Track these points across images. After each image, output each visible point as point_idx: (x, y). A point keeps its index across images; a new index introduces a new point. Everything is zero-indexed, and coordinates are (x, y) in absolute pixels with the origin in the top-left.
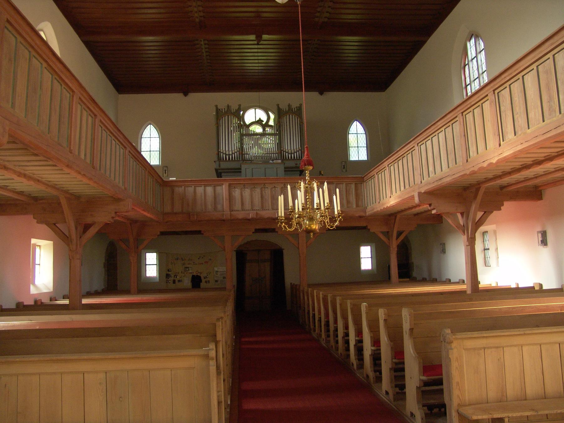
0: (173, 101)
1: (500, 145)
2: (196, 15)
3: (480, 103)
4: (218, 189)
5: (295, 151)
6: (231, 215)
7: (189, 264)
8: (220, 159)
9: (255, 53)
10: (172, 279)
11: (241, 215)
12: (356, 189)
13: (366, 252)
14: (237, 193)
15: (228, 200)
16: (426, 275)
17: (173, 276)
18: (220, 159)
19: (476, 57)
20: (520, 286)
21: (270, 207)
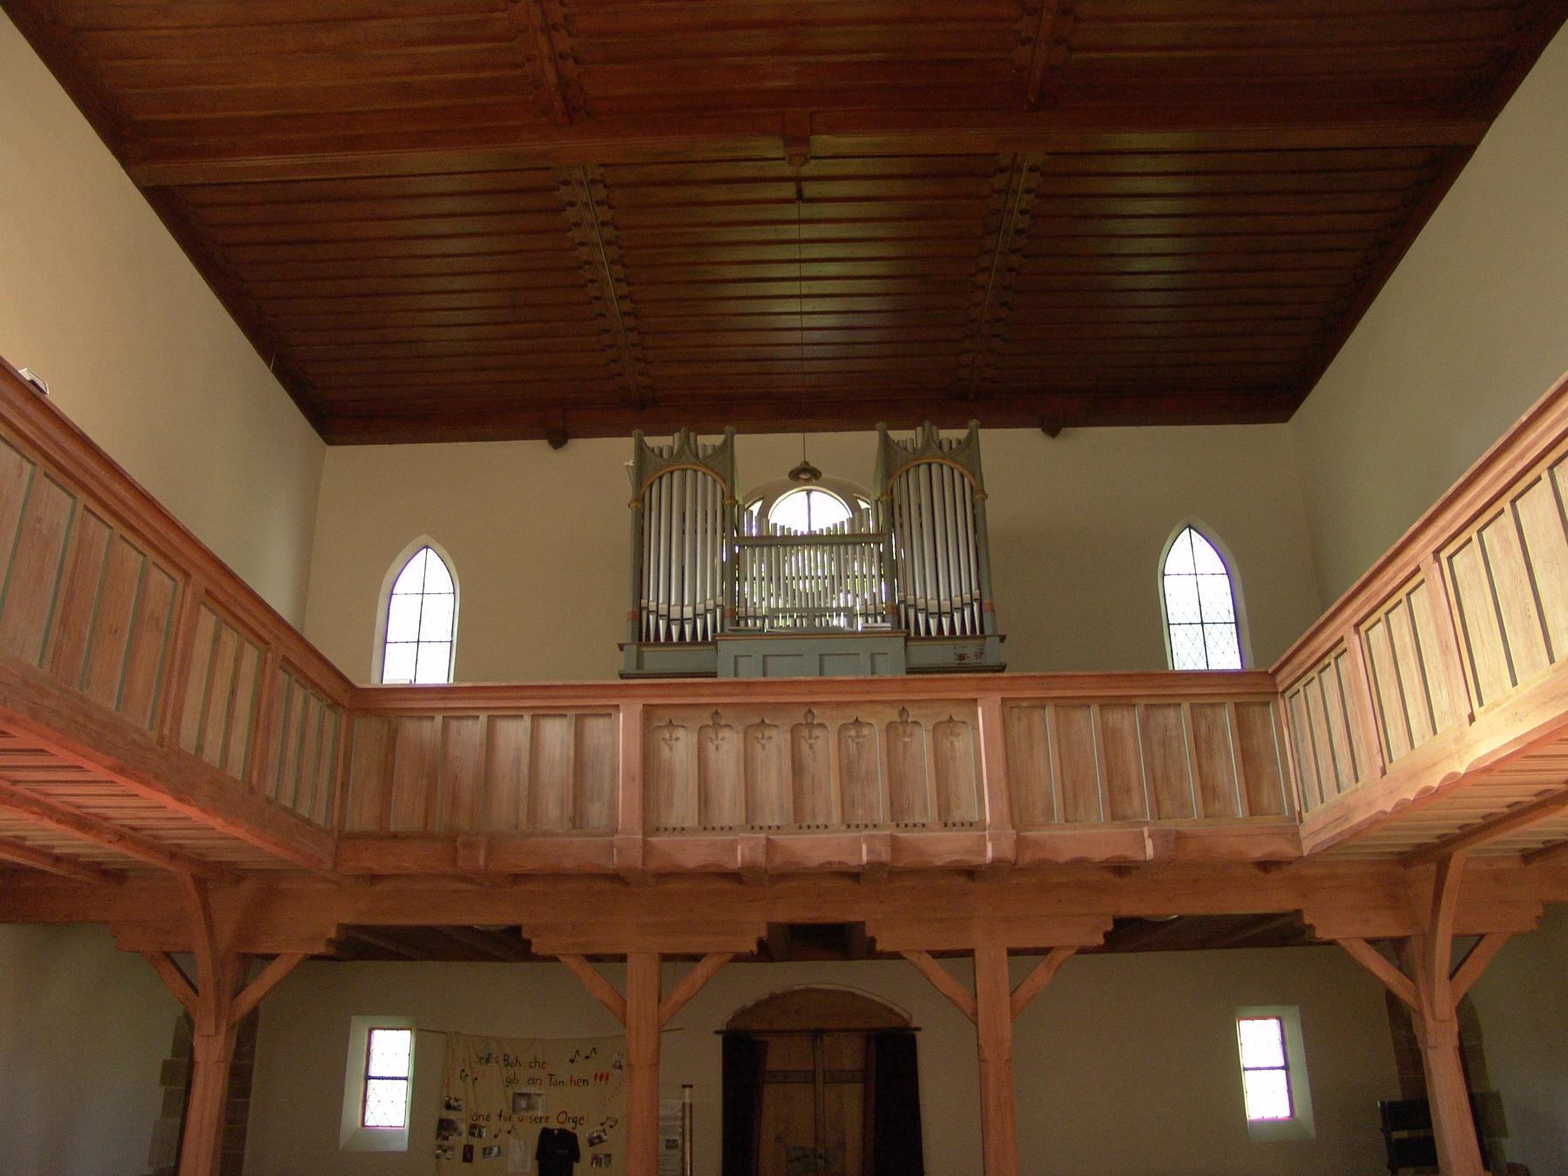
0: (519, 462)
4: (596, 728)
5: (957, 601)
6: (647, 850)
7: (532, 1081)
8: (642, 637)
9: (812, 288)
10: (458, 1141)
11: (693, 853)
12: (1243, 730)
13: (1260, 1042)
14: (680, 749)
15: (638, 781)
17: (463, 1127)
18: (642, 637)
21: (836, 816)
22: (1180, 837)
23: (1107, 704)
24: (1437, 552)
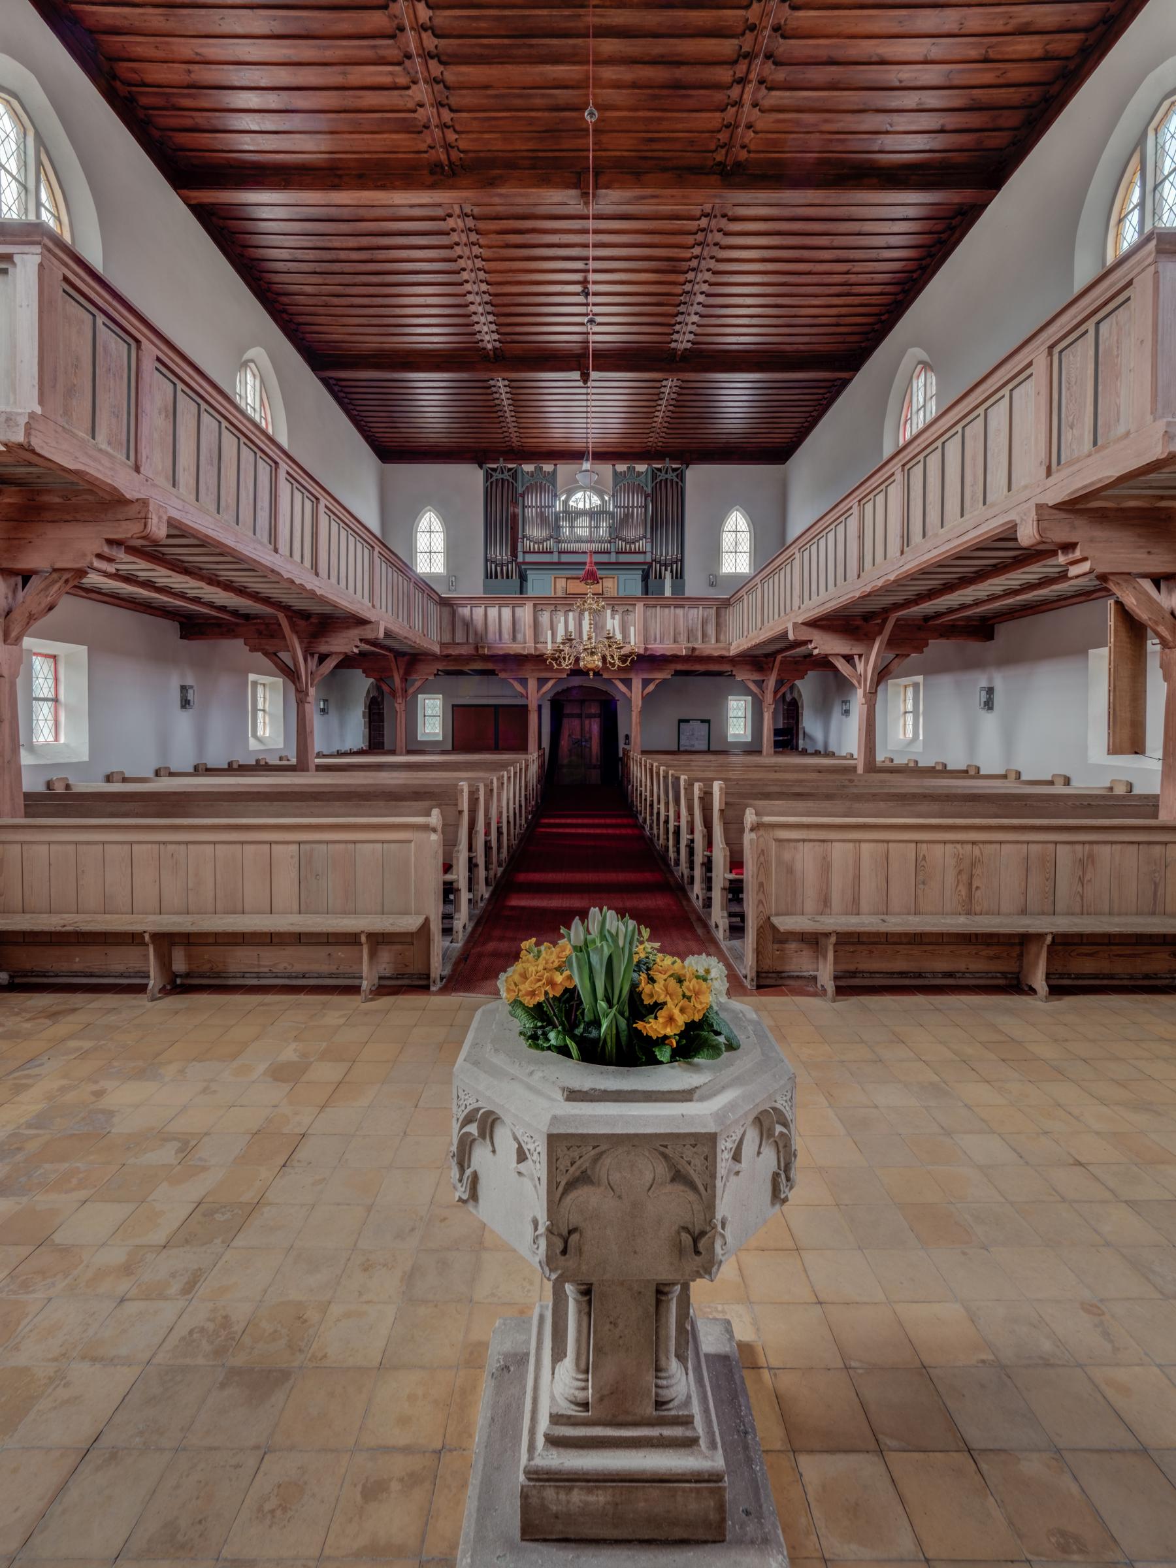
1: (902, 553)
2: (487, 338)
3: (883, 487)
4: (518, 610)
6: (536, 648)
16: (820, 747)
19: (924, 406)
20: (1137, 791)
22: (694, 649)
23: (676, 606)
24: (1051, 347)
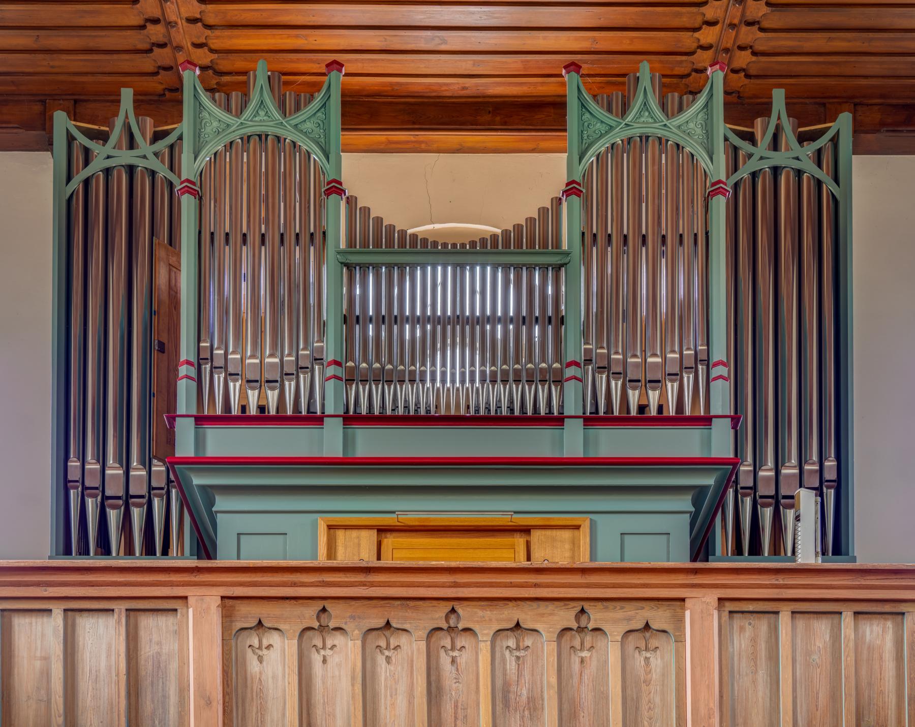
4: (156, 631)
